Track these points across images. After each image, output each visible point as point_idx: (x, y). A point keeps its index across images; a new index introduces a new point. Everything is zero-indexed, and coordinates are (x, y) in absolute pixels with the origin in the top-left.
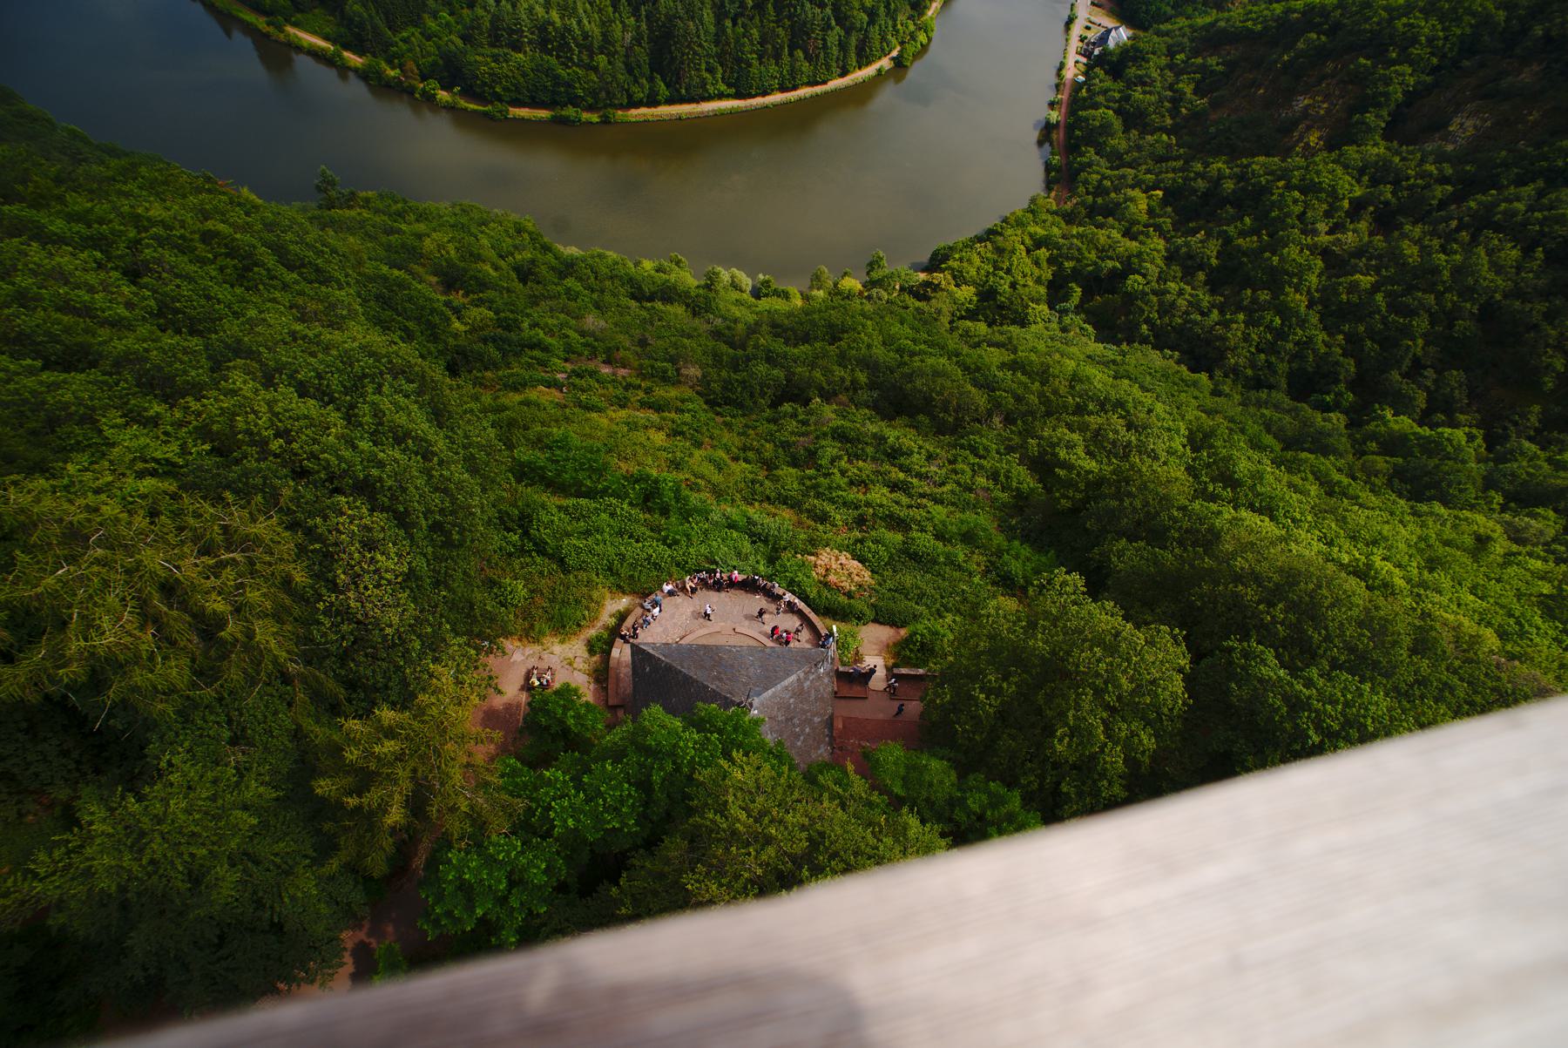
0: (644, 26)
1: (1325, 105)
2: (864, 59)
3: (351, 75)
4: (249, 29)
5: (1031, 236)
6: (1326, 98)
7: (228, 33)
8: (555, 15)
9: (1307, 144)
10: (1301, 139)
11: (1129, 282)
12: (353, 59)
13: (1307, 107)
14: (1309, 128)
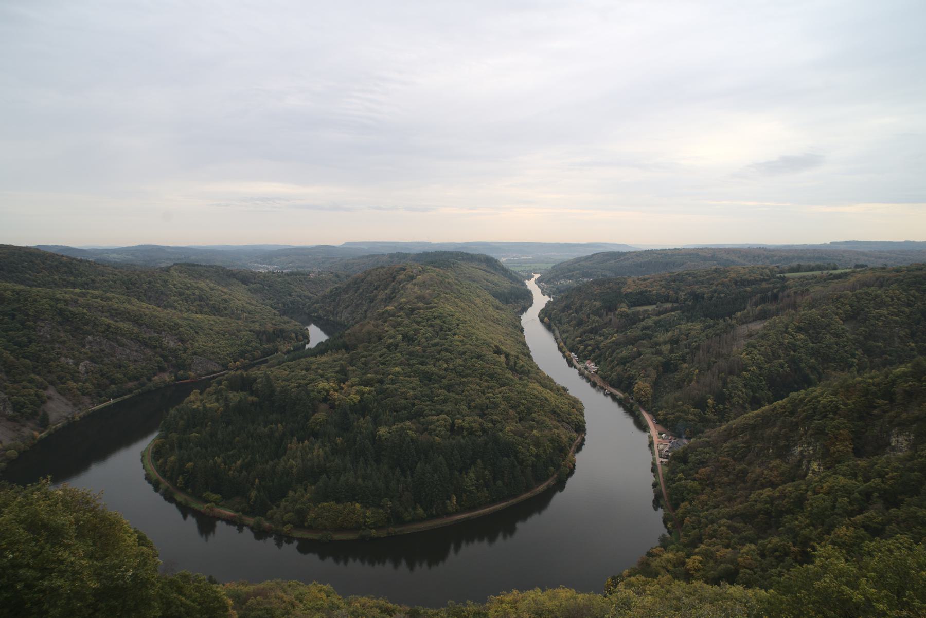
0: (409, 480)
1: (811, 448)
2: (540, 480)
3: (245, 528)
4: (197, 514)
5: (668, 561)
6: (809, 444)
7: (185, 517)
8: (360, 481)
9: (813, 470)
10: (808, 469)
11: (741, 575)
12: (250, 521)
13: (801, 452)
14: (809, 462)
